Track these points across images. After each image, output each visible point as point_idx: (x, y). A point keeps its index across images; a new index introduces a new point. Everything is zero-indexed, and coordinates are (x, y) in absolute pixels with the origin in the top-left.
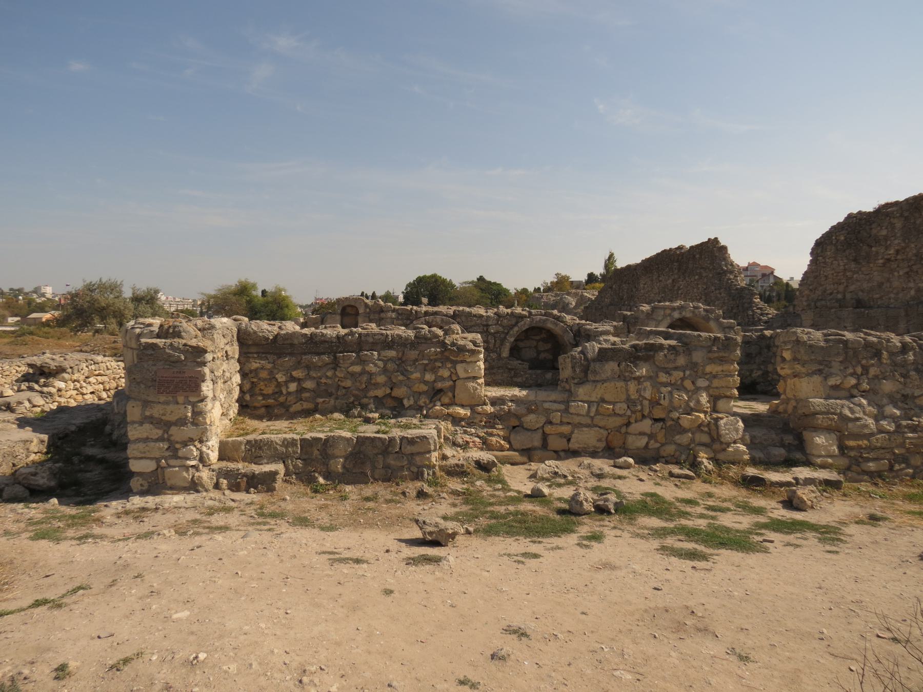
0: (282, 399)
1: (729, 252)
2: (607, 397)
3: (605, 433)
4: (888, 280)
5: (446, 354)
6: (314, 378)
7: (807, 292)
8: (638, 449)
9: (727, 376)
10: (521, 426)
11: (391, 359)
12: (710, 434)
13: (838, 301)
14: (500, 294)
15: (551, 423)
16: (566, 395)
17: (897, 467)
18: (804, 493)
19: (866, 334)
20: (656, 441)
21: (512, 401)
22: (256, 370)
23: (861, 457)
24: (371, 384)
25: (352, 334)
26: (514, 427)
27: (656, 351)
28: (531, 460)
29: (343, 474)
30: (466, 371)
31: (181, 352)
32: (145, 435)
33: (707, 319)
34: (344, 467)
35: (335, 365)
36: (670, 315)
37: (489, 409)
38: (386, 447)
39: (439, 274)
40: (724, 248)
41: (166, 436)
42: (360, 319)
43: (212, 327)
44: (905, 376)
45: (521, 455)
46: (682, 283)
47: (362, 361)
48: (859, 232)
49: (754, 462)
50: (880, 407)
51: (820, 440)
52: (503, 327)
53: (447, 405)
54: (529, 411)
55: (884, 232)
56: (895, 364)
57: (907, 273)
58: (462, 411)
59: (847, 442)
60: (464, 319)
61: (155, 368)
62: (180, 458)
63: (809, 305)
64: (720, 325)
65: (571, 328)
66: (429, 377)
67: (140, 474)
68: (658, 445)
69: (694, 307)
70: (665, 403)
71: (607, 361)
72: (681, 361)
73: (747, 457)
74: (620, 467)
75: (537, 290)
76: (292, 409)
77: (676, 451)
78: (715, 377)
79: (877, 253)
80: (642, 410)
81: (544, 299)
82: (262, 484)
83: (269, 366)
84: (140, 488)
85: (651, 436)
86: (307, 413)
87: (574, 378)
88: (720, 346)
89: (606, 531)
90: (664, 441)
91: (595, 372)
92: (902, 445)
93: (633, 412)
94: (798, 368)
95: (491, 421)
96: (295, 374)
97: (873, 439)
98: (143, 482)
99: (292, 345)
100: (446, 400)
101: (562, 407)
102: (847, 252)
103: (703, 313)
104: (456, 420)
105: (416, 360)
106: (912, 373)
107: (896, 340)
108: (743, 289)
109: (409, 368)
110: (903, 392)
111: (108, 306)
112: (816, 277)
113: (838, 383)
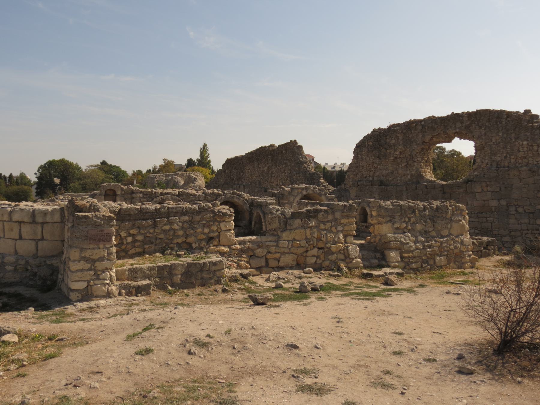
0: (123, 247)
2: (297, 238)
3: (296, 256)
4: (396, 169)
5: (216, 217)
6: (142, 234)
8: (312, 264)
9: (351, 224)
11: (185, 222)
12: (344, 254)
13: (370, 181)
14: (118, 175)
15: (270, 252)
16: (276, 238)
17: (424, 266)
18: (393, 278)
19: (408, 202)
20: (320, 259)
21: (249, 242)
23: (409, 261)
25: (164, 207)
26: (251, 256)
27: (318, 213)
28: (261, 273)
29: (180, 284)
30: (226, 226)
31: (102, 219)
32: (81, 268)
33: (320, 195)
34: (181, 280)
35: (155, 226)
36: (301, 193)
37: (239, 247)
41: (93, 267)
42: (118, 198)
45: (257, 271)
48: (380, 140)
49: (365, 267)
51: (393, 254)
53: (217, 246)
54: (259, 247)
55: (393, 141)
56: (421, 216)
57: (406, 165)
58: (225, 249)
60: (184, 197)
61: (87, 229)
62: (101, 279)
63: (353, 184)
64: (327, 197)
65: (247, 201)
66: (206, 230)
67: (77, 290)
68: (321, 261)
72: (330, 217)
73: (361, 265)
74: (307, 273)
75: (149, 171)
76: (130, 253)
77: (329, 264)
78: (345, 225)
79: (390, 153)
81: (157, 179)
82: (144, 291)
84: (77, 298)
85: (318, 257)
86: (140, 254)
87: (280, 228)
89: (204, 338)
91: (290, 225)
93: (309, 245)
94: (381, 219)
95: (240, 253)
96: (132, 232)
98: (79, 295)
99: (129, 215)
100: (215, 243)
101: (275, 244)
102: (374, 152)
103: (318, 191)
104: (222, 254)
105: (200, 221)
106: (428, 220)
107: (421, 204)
108: (313, 173)
109: (196, 226)
112: (357, 167)
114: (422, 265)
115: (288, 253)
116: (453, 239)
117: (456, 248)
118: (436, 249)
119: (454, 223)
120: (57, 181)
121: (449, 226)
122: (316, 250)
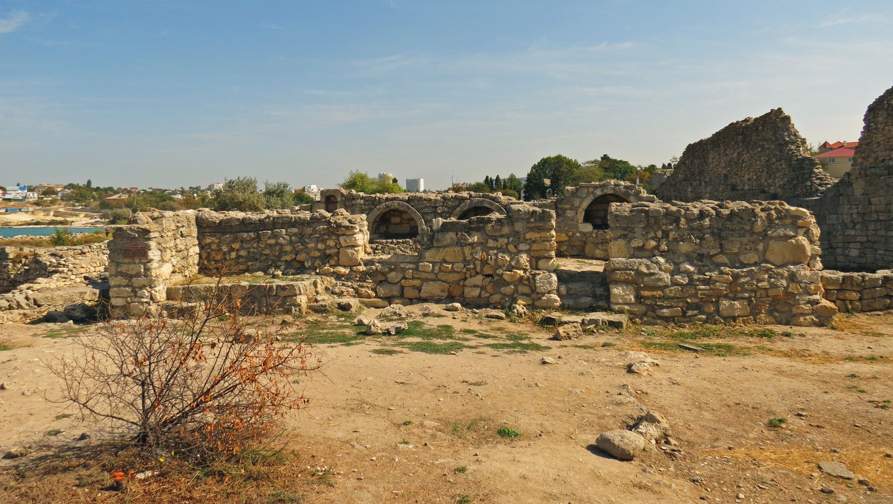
1: (792, 122)
2: (448, 259)
7: (860, 160)
10: (386, 281)
11: (295, 235)
15: (406, 278)
22: (210, 244)
24: (282, 252)
26: (381, 282)
31: (136, 232)
35: (258, 239)
36: (593, 193)
38: (266, 292)
39: (564, 155)
40: (788, 118)
43: (163, 216)
44: (702, 239)
46: (746, 156)
47: (275, 236)
50: (677, 264)
52: (448, 208)
54: (391, 270)
56: (691, 229)
58: (342, 270)
59: (642, 293)
63: (860, 174)
66: (320, 246)
68: (488, 295)
69: (615, 185)
70: (492, 263)
71: (447, 232)
72: (506, 230)
80: (475, 268)
83: (217, 241)
85: (483, 288)
88: (537, 218)
90: (492, 291)
92: (695, 295)
95: (364, 276)
97: (667, 291)
99: (231, 226)
104: (338, 276)
110: (699, 251)
111: (245, 201)
112: (868, 144)
113: (640, 245)
114: (684, 313)
115: (433, 280)
116: (768, 270)
117: (773, 286)
118: (722, 287)
119: (772, 242)
120: (547, 182)
121: (761, 247)
122: (480, 277)
